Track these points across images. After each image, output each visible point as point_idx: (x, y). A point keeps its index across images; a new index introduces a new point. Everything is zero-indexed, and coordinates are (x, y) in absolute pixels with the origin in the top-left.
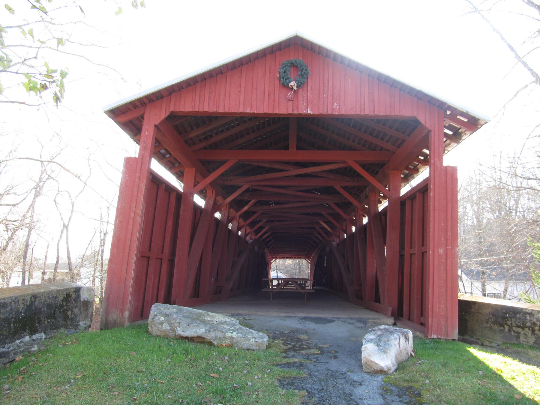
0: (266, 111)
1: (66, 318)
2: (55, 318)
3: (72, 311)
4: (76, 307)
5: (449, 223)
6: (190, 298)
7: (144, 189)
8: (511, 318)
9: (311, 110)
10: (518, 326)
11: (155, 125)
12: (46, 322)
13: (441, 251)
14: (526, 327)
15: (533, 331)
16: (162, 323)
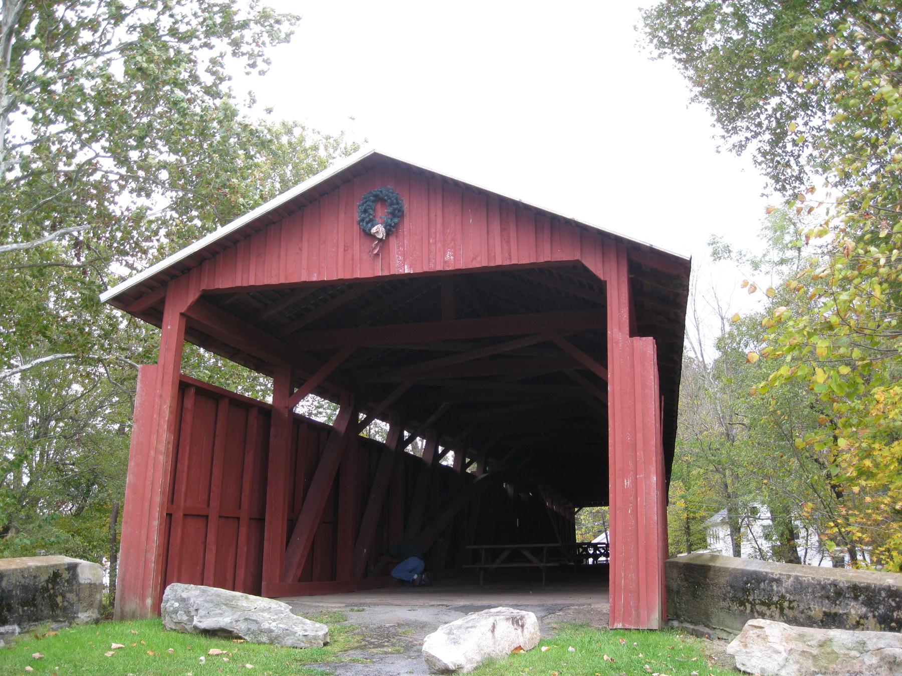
0: (341, 276)
1: (54, 606)
2: (35, 606)
3: (64, 597)
4: (71, 591)
5: (639, 436)
6: (299, 581)
7: (168, 412)
8: (753, 590)
9: (410, 267)
10: (763, 603)
11: (181, 314)
12: (20, 610)
13: (627, 483)
14: (773, 604)
15: (782, 609)
16: (176, 611)
